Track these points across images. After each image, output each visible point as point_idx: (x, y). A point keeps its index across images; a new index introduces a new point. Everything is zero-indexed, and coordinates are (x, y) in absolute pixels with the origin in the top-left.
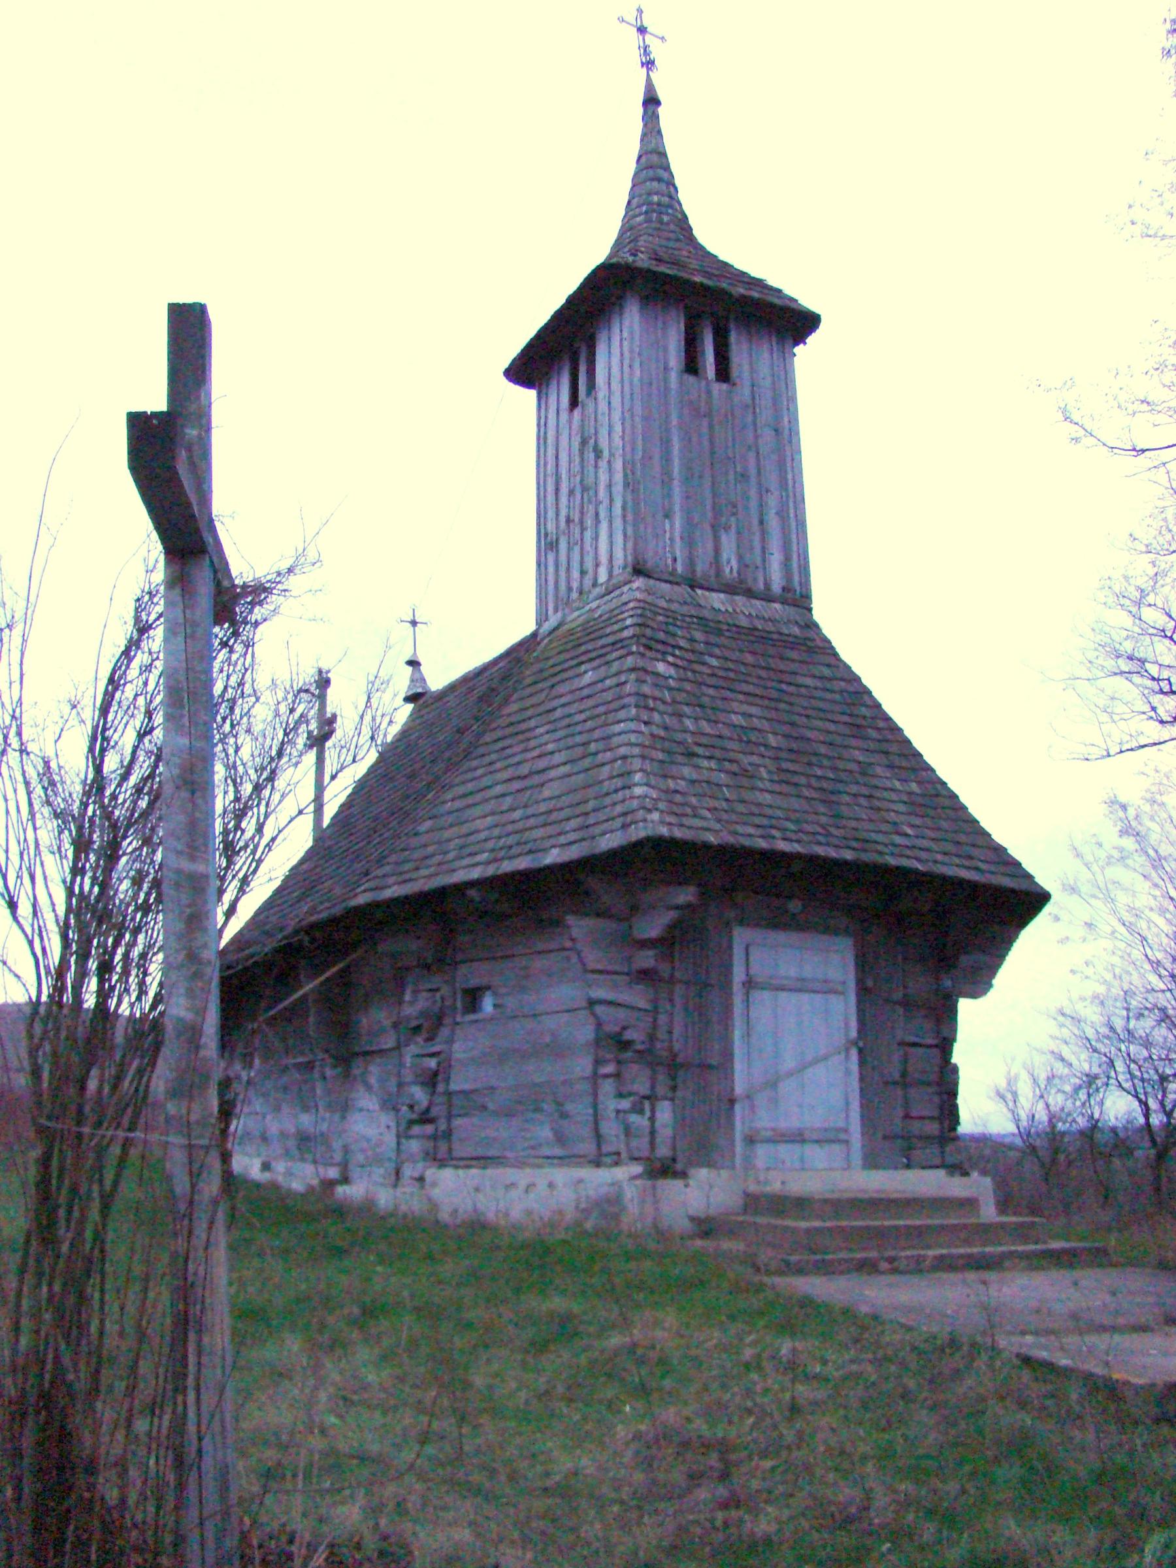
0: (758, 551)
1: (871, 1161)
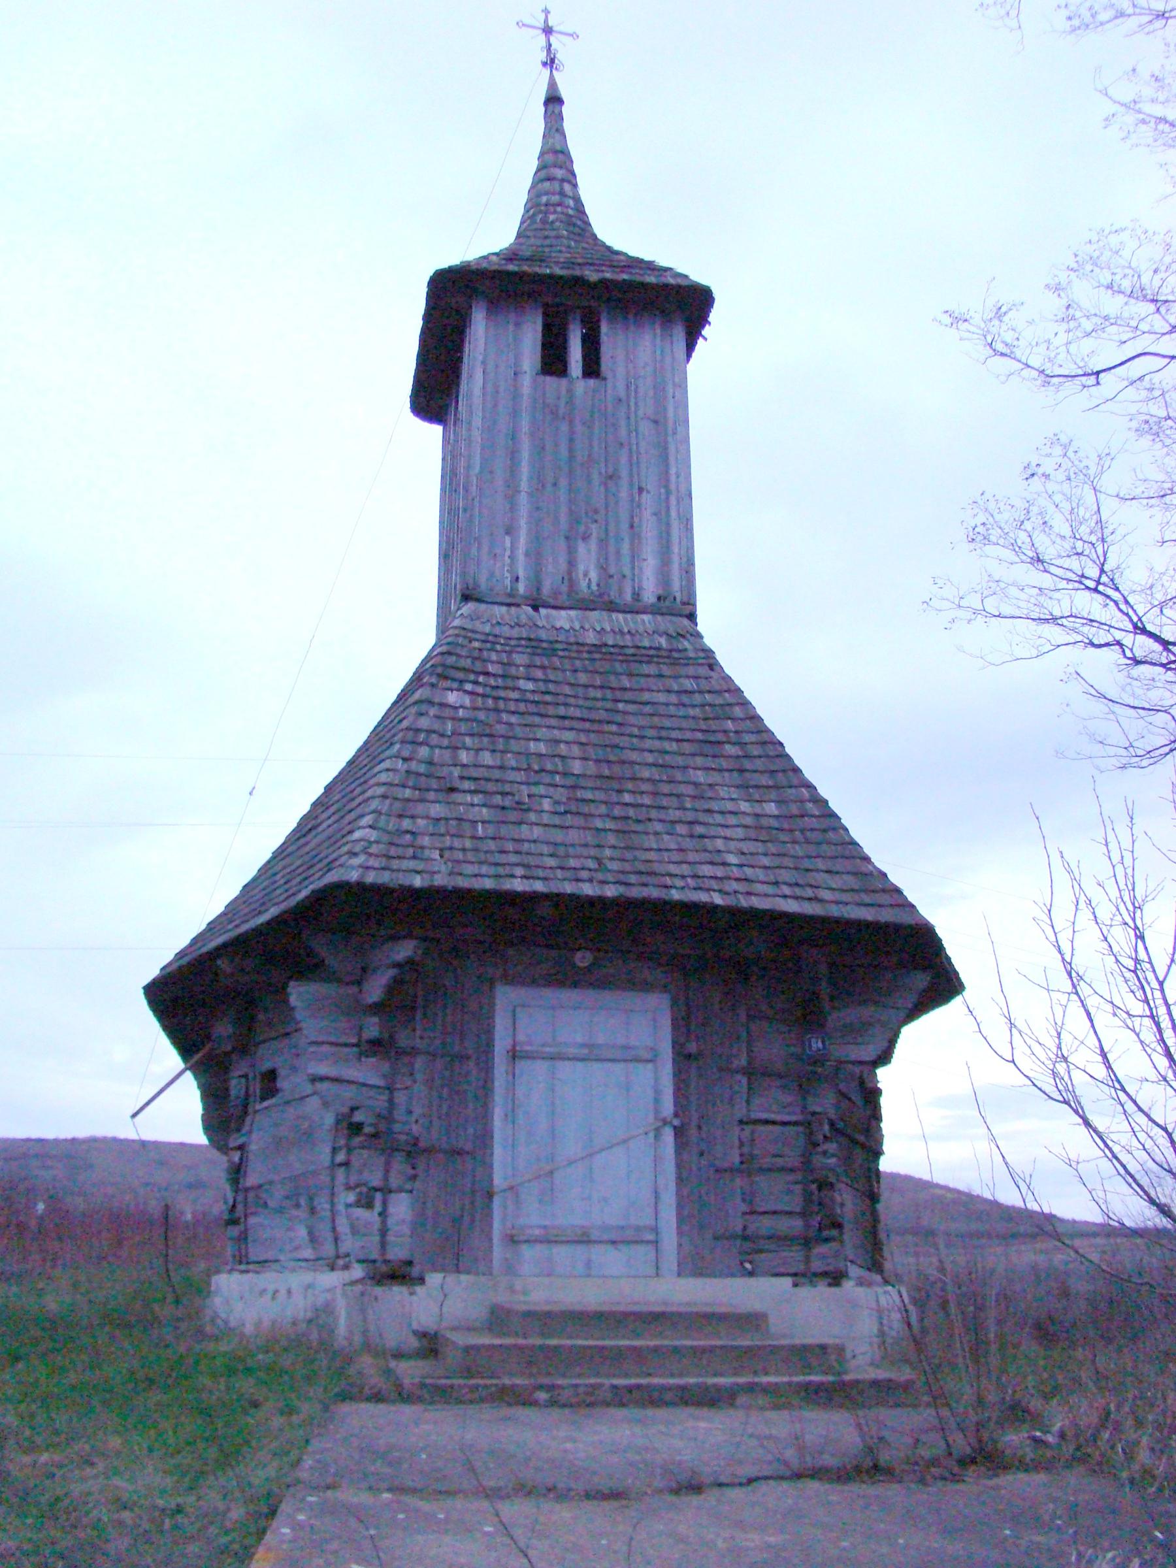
0: (626, 559)
1: (694, 1265)
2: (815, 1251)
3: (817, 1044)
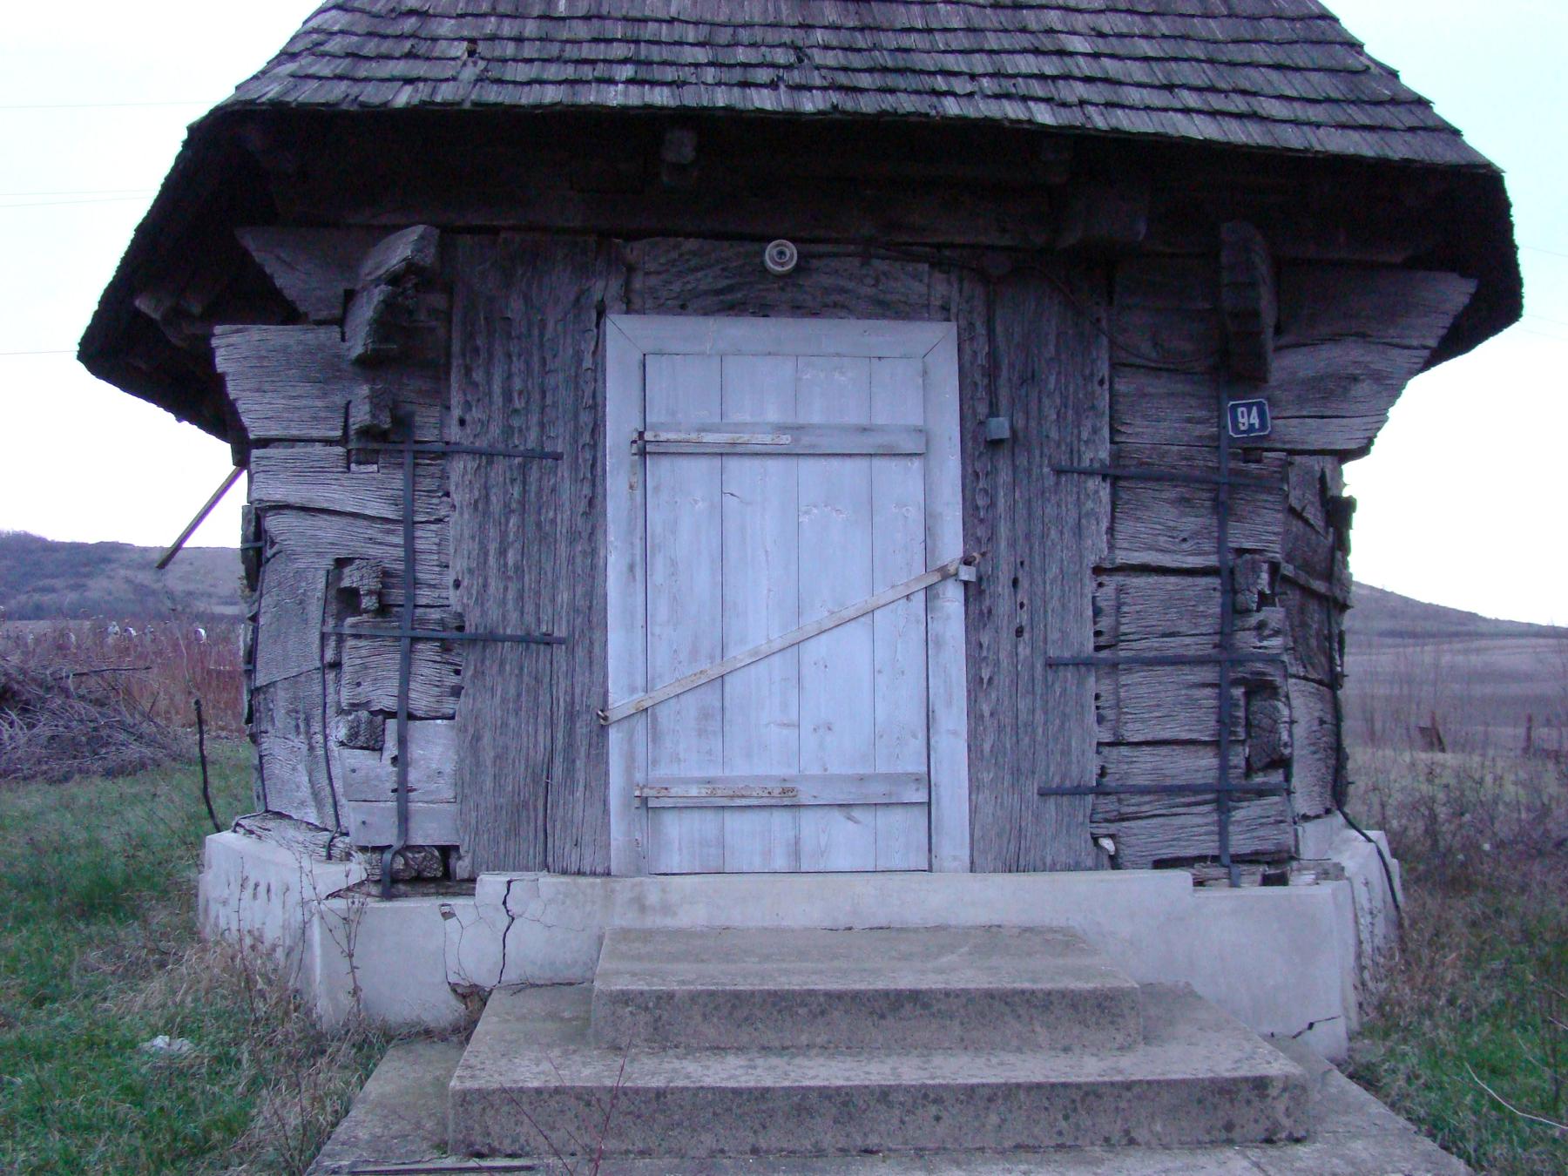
1: (1007, 851)
2: (1238, 815)
3: (1248, 419)
